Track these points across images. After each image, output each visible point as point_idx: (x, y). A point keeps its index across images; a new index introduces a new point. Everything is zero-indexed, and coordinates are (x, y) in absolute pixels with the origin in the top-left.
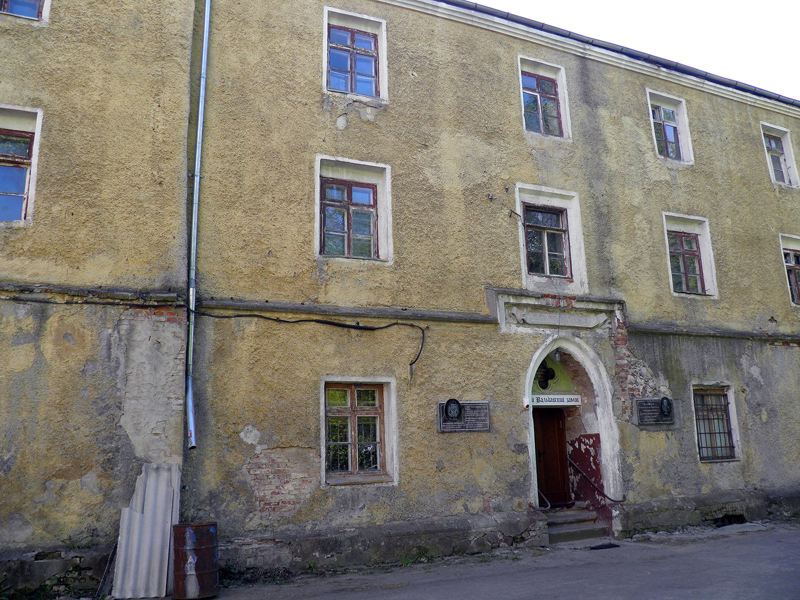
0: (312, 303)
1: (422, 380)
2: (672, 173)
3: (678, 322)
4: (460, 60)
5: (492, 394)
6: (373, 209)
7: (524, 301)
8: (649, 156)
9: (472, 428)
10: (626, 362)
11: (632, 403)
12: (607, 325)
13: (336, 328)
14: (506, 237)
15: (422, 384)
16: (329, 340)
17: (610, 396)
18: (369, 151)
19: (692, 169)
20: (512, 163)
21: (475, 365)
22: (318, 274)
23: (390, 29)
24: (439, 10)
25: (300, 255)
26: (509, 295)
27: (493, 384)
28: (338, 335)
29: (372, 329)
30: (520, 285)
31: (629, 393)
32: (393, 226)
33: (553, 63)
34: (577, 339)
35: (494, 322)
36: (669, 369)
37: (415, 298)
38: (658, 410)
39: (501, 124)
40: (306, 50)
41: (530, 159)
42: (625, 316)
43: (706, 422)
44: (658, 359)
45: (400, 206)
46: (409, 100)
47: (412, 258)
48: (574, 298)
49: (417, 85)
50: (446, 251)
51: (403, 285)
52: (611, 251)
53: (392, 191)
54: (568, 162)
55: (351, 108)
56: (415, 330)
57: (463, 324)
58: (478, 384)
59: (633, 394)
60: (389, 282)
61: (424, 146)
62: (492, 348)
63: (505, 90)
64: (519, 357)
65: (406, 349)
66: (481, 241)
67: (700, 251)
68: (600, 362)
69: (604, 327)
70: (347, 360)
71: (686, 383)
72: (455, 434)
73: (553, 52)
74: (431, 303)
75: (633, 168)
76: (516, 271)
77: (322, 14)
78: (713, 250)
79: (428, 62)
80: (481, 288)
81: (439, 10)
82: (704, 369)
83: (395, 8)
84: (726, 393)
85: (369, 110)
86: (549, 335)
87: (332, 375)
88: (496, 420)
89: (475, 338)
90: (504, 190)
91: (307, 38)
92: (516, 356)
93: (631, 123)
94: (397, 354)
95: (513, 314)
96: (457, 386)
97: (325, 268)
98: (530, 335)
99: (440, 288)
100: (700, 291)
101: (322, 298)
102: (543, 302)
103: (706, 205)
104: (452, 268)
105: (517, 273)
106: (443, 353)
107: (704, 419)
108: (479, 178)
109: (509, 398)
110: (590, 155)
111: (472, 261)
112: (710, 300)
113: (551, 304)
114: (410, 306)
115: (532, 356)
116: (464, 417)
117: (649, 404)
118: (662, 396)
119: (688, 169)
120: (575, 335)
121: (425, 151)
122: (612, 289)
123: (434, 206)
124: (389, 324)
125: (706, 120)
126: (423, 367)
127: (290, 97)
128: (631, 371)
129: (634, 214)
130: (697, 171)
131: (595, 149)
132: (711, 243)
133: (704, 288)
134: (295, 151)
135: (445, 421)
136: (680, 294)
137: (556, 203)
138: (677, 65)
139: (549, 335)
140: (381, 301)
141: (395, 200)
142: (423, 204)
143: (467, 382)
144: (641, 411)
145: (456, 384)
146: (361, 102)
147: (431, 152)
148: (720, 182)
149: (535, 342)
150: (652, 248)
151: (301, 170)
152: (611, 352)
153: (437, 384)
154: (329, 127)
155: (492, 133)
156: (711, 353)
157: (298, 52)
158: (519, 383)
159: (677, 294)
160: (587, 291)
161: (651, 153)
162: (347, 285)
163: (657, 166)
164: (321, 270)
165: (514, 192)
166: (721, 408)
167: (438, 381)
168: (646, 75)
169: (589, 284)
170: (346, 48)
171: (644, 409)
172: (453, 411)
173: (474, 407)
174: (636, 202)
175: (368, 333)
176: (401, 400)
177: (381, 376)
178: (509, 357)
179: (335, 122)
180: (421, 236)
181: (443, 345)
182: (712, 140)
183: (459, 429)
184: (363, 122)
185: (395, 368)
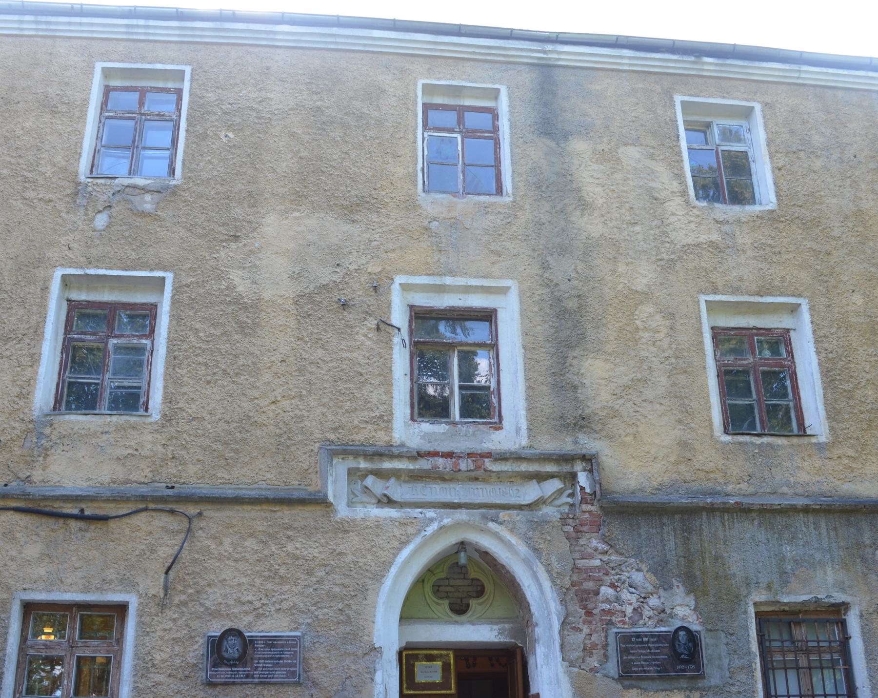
0: (21, 484)
1: (183, 597)
2: (726, 228)
3: (730, 488)
4: (311, 103)
5: (310, 621)
6: (147, 339)
7: (387, 465)
8: (675, 205)
9: (267, 678)
10: (597, 563)
11: (606, 637)
12: (564, 499)
13: (44, 520)
14: (368, 364)
15: (184, 604)
16: (34, 537)
17: (556, 626)
18: (141, 256)
19: (771, 217)
20: (390, 246)
21: (282, 571)
22: (35, 440)
23: (197, 77)
24: (278, 37)
25: (10, 414)
26: (356, 455)
27: (315, 604)
28: (48, 529)
29: (105, 519)
30: (387, 438)
31: (601, 620)
32: (166, 362)
33: (484, 82)
34: (492, 525)
35: (320, 501)
36: (698, 573)
37: (192, 469)
38: (666, 651)
39: (375, 189)
40: (60, 127)
41: (425, 236)
42: (594, 482)
43: (792, 675)
44: (671, 556)
45: (182, 331)
46: (215, 173)
47: (193, 409)
48: (489, 455)
49: (233, 150)
50: (255, 393)
51: (173, 451)
52: (582, 371)
53: (172, 310)
54: (500, 232)
55: (117, 198)
56: (178, 518)
57: (265, 507)
58: (285, 605)
59: (610, 620)
60: (149, 446)
61: (232, 238)
62: (317, 544)
63: (388, 136)
64: (369, 557)
65: (161, 549)
66: (321, 373)
67: (793, 358)
68: (539, 564)
69: (558, 502)
70: (60, 566)
71: (737, 600)
72: (234, 688)
73: (487, 65)
74: (219, 475)
75: (637, 228)
76: (381, 417)
77: (92, 73)
78: (818, 353)
79: (255, 115)
80: (312, 448)
81: (278, 37)
82: (783, 573)
83: (209, 46)
84: (844, 617)
85: (148, 197)
86: (431, 520)
87: (32, 590)
88: (314, 666)
89: (287, 529)
90: (372, 289)
91: (64, 110)
92: (363, 556)
93: (638, 156)
94: (145, 557)
95: (366, 488)
96: (246, 608)
97: (47, 431)
98: (393, 520)
99: (236, 451)
100: (796, 431)
101: (37, 475)
102: (424, 464)
103: (803, 275)
104: (261, 418)
105: (385, 420)
106: (225, 554)
107: (810, 668)
108: (326, 275)
109: (342, 628)
110: (545, 218)
111: (301, 407)
112: (809, 444)
113: (441, 467)
114: (183, 481)
115: (395, 556)
116: (252, 659)
117: (645, 639)
118: (679, 624)
119: (762, 218)
120: (487, 518)
121: (233, 246)
122: (581, 436)
123: (242, 328)
124: (134, 509)
125: (809, 131)
126: (187, 577)
127: (28, 194)
128: (607, 579)
129: (636, 306)
130: (782, 219)
131: (559, 207)
132: (812, 340)
133: (803, 424)
134: (25, 268)
135: (215, 665)
136: (735, 437)
137: (476, 301)
138: (871, 61)
139: (431, 520)
140: (134, 477)
141: (174, 322)
142: (224, 325)
143: (265, 601)
144: (624, 652)
145: (244, 604)
146: (135, 187)
147: (245, 245)
148: (836, 232)
149: (404, 533)
150: (673, 360)
151: (29, 293)
152: (564, 546)
153: (208, 603)
154: (80, 228)
155: (358, 205)
156: (801, 542)
157: (48, 130)
158: (364, 602)
159: (728, 438)
160: (524, 442)
161: (679, 200)
162: (80, 455)
163: (692, 219)
164: (40, 435)
165: (389, 291)
166: (830, 647)
167: (214, 597)
168: (675, 74)
169: (529, 429)
170: (131, 115)
171: (632, 648)
172: (232, 648)
173: (271, 642)
174: (640, 284)
175: (99, 525)
176: (144, 630)
177: (114, 591)
178: (349, 558)
179: (92, 220)
180: (214, 374)
181: (227, 541)
182: (818, 164)
183: (242, 678)
184: (135, 214)
185: (138, 580)
